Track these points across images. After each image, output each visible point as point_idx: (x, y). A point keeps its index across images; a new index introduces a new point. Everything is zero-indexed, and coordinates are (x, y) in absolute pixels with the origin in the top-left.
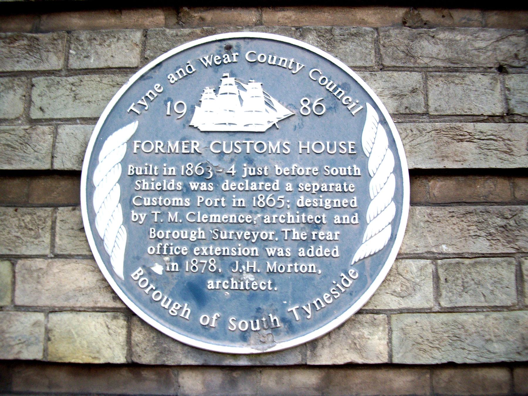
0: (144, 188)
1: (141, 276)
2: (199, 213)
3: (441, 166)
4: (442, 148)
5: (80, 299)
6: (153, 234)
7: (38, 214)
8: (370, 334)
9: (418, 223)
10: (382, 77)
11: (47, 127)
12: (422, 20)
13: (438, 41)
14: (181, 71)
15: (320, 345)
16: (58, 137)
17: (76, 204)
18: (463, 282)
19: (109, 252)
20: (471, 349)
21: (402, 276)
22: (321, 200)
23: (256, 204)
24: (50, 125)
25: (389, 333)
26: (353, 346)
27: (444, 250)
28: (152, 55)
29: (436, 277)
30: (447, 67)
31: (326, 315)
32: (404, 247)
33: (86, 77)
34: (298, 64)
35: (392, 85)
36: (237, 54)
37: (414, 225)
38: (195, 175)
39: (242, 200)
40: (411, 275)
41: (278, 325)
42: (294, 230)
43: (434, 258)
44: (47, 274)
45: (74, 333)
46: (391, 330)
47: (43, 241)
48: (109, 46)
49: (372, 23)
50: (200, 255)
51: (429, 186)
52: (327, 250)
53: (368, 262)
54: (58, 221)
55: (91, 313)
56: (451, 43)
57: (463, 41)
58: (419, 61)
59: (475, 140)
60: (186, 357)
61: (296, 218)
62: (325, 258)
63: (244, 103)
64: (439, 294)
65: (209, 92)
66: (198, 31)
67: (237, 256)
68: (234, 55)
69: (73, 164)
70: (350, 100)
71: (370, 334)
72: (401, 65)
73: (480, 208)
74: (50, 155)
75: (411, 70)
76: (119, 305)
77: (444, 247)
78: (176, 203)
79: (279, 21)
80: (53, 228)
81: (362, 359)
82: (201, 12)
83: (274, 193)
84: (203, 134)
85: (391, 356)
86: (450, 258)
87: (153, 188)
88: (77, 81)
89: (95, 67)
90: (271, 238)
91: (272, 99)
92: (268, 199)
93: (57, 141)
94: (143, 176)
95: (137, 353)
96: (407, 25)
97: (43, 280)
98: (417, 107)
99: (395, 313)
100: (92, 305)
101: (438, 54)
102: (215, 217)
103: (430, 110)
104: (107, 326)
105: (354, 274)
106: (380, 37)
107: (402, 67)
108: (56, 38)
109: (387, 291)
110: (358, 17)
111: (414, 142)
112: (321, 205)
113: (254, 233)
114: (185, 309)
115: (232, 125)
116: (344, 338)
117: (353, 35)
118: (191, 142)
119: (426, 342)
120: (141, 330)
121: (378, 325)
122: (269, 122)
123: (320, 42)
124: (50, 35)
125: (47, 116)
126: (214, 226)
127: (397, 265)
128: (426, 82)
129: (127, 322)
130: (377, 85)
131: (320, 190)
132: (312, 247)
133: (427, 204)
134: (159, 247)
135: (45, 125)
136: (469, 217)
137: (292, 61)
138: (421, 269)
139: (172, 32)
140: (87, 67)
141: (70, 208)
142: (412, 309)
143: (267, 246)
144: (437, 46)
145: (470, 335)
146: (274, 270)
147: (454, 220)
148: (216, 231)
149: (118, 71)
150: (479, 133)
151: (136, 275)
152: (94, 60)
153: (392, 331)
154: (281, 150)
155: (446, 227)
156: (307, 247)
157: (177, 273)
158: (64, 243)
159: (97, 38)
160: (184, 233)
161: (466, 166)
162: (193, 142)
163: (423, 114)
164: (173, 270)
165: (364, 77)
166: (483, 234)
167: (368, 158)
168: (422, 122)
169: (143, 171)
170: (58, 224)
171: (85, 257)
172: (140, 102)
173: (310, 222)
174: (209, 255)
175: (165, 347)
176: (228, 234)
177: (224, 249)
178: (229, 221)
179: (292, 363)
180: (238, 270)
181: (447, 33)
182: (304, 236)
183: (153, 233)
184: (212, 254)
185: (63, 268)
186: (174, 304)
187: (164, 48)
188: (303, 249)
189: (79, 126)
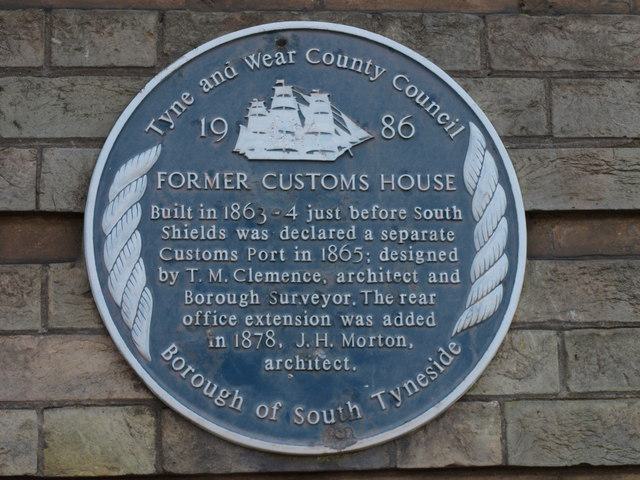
0: (174, 237)
3: (568, 207)
4: (571, 182)
6: (189, 299)
7: (21, 273)
8: (478, 427)
13: (568, 34)
15: (413, 443)
17: (76, 256)
18: (598, 360)
20: (610, 446)
22: (411, 252)
28: (173, 49)
29: (563, 354)
31: (422, 401)
32: (521, 313)
33: (80, 79)
39: (307, 255)
43: (560, 328)
46: (504, 423)
47: (30, 311)
48: (111, 34)
49: (476, 6)
53: (473, 333)
54: (50, 283)
56: (584, 38)
57: (601, 34)
58: (540, 63)
59: (615, 172)
61: (378, 276)
63: (306, 122)
65: (257, 106)
66: (237, 16)
68: (290, 53)
70: (448, 118)
71: (478, 427)
73: (622, 262)
76: (142, 395)
77: (573, 313)
80: (44, 292)
84: (251, 164)
85: (505, 456)
87: (186, 237)
90: (346, 303)
91: (343, 116)
92: (341, 251)
96: (525, 8)
100: (105, 396)
101: (567, 53)
102: (272, 275)
104: (128, 425)
105: (456, 348)
107: (517, 71)
108: (29, 19)
112: (411, 259)
117: (451, 26)
122: (340, 148)
124: (19, 13)
126: (271, 287)
131: (409, 238)
132: (401, 314)
134: (198, 316)
135: (23, 147)
136: (606, 275)
137: (369, 63)
140: (80, 65)
141: (68, 264)
143: (341, 313)
144: (565, 41)
145: (609, 428)
146: (351, 343)
147: (586, 278)
150: (621, 163)
156: (394, 314)
158: (63, 312)
160: (232, 296)
161: (601, 206)
162: (238, 174)
164: (218, 345)
166: (626, 297)
167: (472, 197)
169: (172, 213)
170: (51, 286)
171: (92, 332)
172: (162, 118)
174: (266, 325)
176: (290, 298)
177: (285, 317)
179: (377, 466)
180: (305, 345)
181: (579, 23)
182: (390, 300)
185: (62, 347)
186: (222, 391)
189: (74, 149)
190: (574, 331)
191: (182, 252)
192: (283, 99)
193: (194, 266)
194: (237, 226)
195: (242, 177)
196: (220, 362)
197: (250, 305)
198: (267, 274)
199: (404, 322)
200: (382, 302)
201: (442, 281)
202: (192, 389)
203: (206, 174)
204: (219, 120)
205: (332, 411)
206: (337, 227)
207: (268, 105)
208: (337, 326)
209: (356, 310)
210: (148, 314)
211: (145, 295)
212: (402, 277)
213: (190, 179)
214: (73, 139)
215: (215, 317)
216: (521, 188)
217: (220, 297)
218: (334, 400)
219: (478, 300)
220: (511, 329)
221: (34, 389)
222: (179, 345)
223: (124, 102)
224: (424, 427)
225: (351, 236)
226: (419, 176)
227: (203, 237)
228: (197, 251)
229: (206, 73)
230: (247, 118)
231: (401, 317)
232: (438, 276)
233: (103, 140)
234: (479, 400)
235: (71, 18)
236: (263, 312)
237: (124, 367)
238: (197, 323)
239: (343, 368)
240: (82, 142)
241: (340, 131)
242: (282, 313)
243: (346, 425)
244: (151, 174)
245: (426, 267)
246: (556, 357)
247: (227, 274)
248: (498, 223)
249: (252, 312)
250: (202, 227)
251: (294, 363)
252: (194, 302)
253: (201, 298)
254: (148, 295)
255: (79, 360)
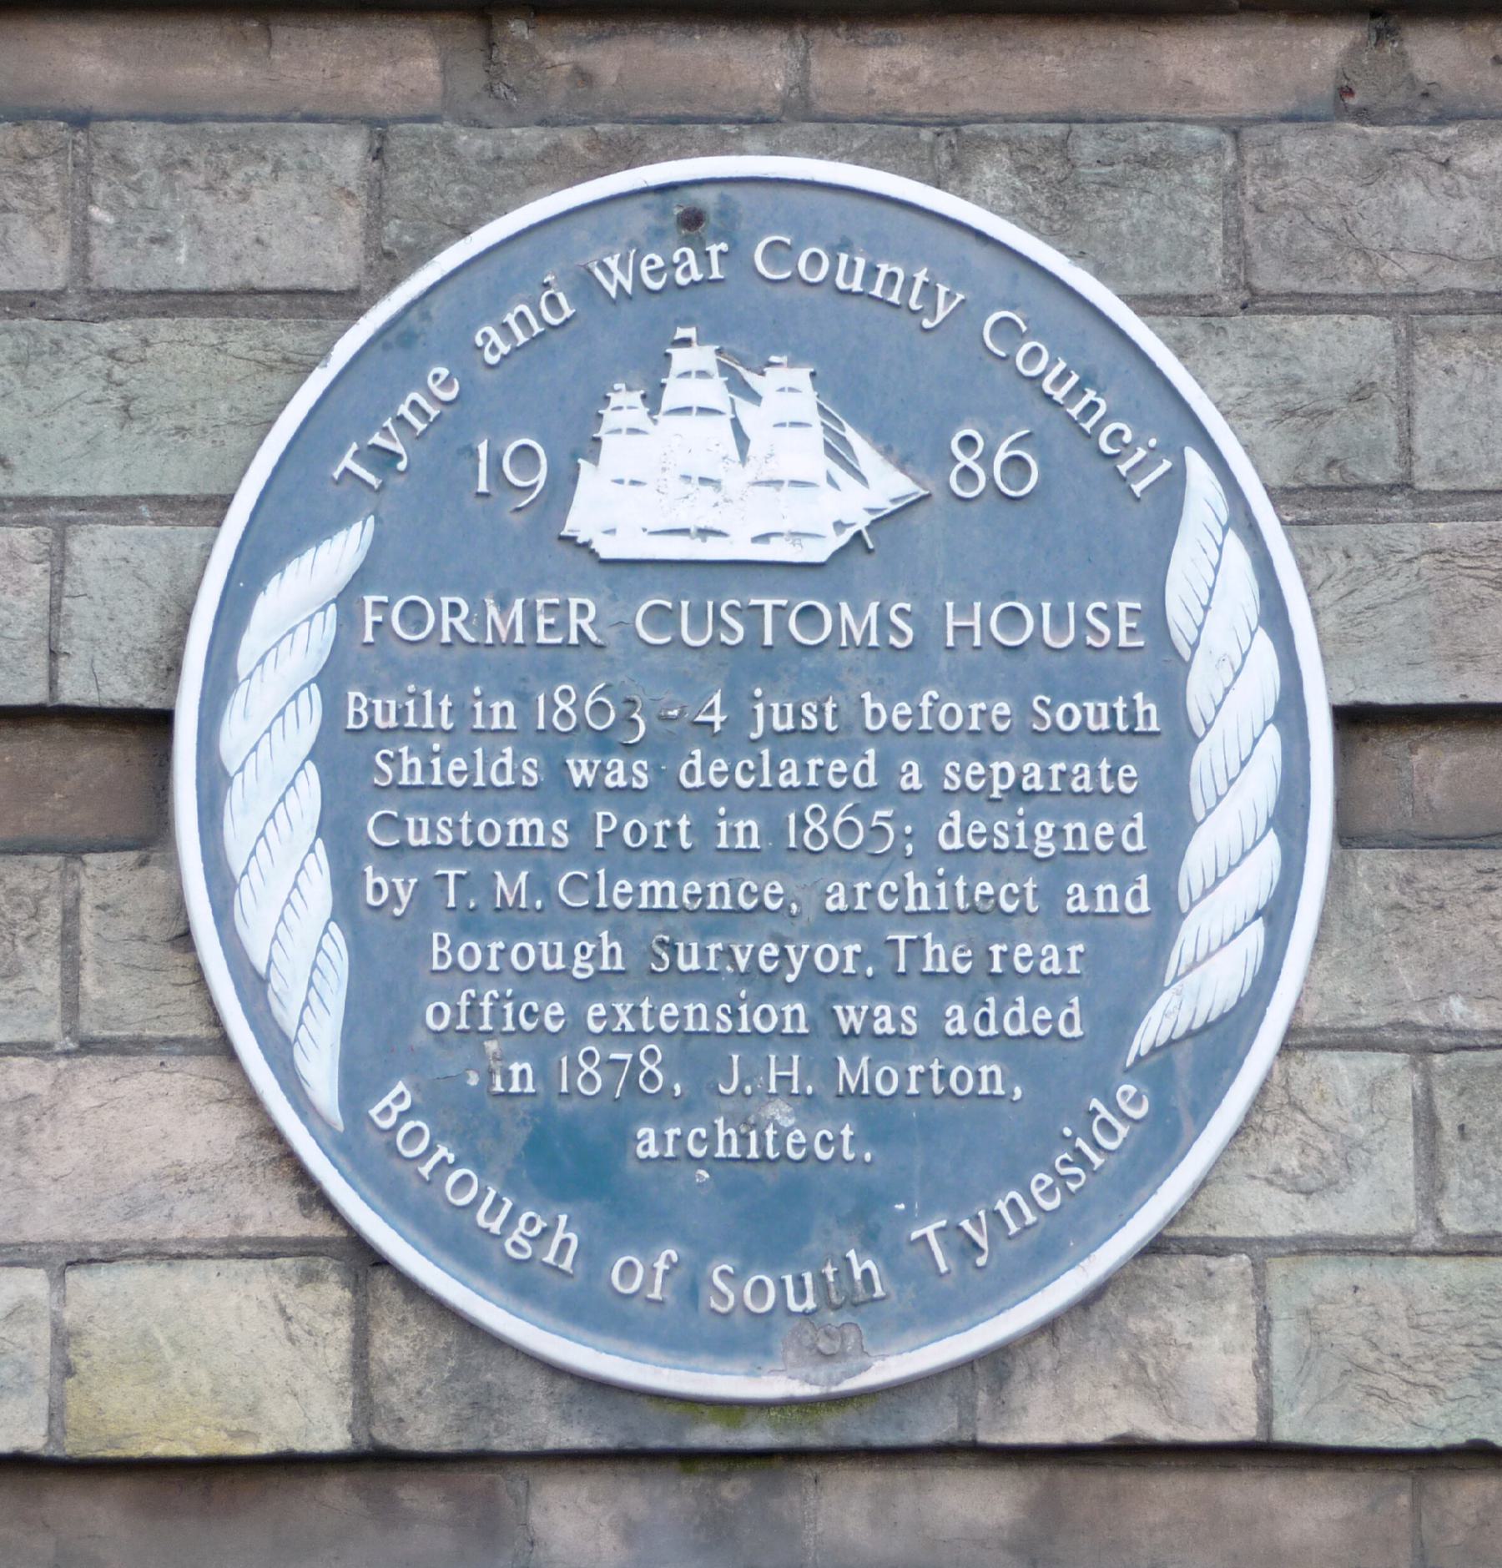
0: (405, 781)
1: (404, 1116)
2: (601, 872)
3: (1449, 694)
4: (1459, 621)
5: (181, 1209)
9: (1364, 910)
10: (1245, 339)
11: (26, 532)
12: (1412, 80)
13: (1463, 180)
14: (521, 315)
15: (1021, 1372)
16: (68, 572)
17: (151, 834)
19: (289, 1024)
21: (1303, 1112)
22: (1021, 825)
23: (799, 838)
24: (36, 522)
25: (1259, 1326)
26: (1132, 1374)
27: (1457, 1018)
29: (1426, 1120)
30: (1489, 294)
31: (1045, 1252)
33: (164, 328)
34: (943, 290)
35: (1282, 370)
36: (724, 246)
37: (1349, 918)
38: (583, 728)
39: (747, 831)
40: (1336, 1108)
41: (879, 1292)
42: (928, 937)
44: (54, 1115)
45: (162, 1341)
46: (1265, 1318)
47: (33, 989)
48: (244, 195)
49: (1223, 99)
50: (607, 1030)
51: (1411, 770)
52: (1043, 1012)
53: (1183, 1058)
54: (86, 908)
55: (222, 1263)
60: (566, 1418)
61: (934, 893)
62: (1033, 1042)
64: (1438, 1184)
65: (624, 406)
66: (575, 139)
67: (734, 1033)
68: (714, 249)
69: (135, 684)
70: (1127, 438)
71: (1197, 1329)
72: (1319, 289)
74: (45, 643)
75: (1355, 305)
76: (320, 1228)
77: (1457, 1005)
78: (519, 837)
79: (871, 92)
80: (69, 936)
81: (1167, 1423)
82: (579, 43)
83: (859, 800)
85: (1266, 1415)
86: (1477, 1048)
87: (437, 781)
88: (132, 341)
89: (194, 284)
90: (849, 968)
91: (850, 434)
92: (839, 820)
93: (67, 588)
94: (401, 734)
95: (391, 1411)
96: (1353, 102)
97: (39, 1140)
98: (1370, 461)
99: (1281, 1251)
100: (223, 1231)
102: (659, 890)
103: (1418, 471)
104: (282, 1310)
105: (1136, 1101)
106: (1247, 171)
108: (32, 151)
109: (1253, 1171)
110: (1170, 71)
111: (1359, 601)
112: (1021, 845)
113: (790, 949)
114: (559, 1236)
115: (711, 539)
116: (1105, 1342)
117: (1144, 162)
118: (568, 603)
119: (1389, 1365)
120: (404, 1321)
121: (1222, 1296)
122: (839, 526)
123: (1024, 194)
125: (22, 488)
127: (1287, 1072)
128: (1409, 355)
129: (354, 1293)
130: (1226, 372)
132: (991, 1000)
133: (1401, 842)
134: (464, 1003)
137: (921, 276)
138: (1373, 1088)
139: (479, 142)
140: (164, 286)
141: (132, 857)
142: (1342, 1239)
143: (836, 998)
144: (1456, 204)
146: (860, 1085)
148: (662, 943)
149: (283, 302)
151: (387, 1110)
152: (191, 256)
153: (1270, 1319)
154: (882, 636)
155: (1465, 931)
156: (973, 1003)
157: (529, 1099)
158: (117, 995)
159: (195, 159)
160: (552, 948)
162: (574, 602)
163: (1392, 486)
165: (1180, 340)
168: (1388, 520)
169: (401, 713)
171: (192, 1047)
172: (377, 439)
173: (981, 906)
174: (639, 1032)
175: (488, 1384)
176: (703, 953)
177: (690, 1008)
178: (705, 903)
179: (925, 1435)
180: (740, 1088)
182: (963, 960)
183: (445, 949)
184: (647, 1028)
187: (451, 210)
188: (960, 1009)
189: (148, 529)
190: (1457, 1056)
191: (425, 821)
192: (693, 383)
193: (457, 863)
194: (568, 748)
195: (583, 609)
196: (521, 1135)
197: (599, 972)
198: (645, 886)
199: (999, 1023)
200: (943, 968)
201: (1101, 908)
202: (445, 1210)
203: (489, 602)
204: (525, 447)
205: (808, 1277)
206: (829, 754)
207: (652, 401)
208: (824, 1040)
209: (875, 988)
210: (336, 999)
211: (328, 945)
212: (996, 896)
213: (447, 618)
214: (145, 498)
215: (509, 1006)
216: (1322, 642)
217: (523, 952)
218: (815, 1246)
219: (1195, 964)
220: (1286, 1048)
221: (42, 1210)
222: (416, 1088)
223: (278, 395)
224: (1049, 1327)
225: (865, 778)
226: (1046, 606)
227: (480, 782)
228: (465, 820)
229: (493, 312)
230: (598, 440)
231: (991, 1011)
232: (1091, 894)
233: (224, 502)
234: (1200, 1252)
235: (141, 147)
236: (634, 993)
237: (274, 1150)
238: (463, 1025)
239: (838, 1154)
240: (171, 507)
241: (840, 474)
242: (681, 996)
243: (847, 1317)
244: (347, 599)
245: (1060, 867)
246: (1409, 1130)
247: (541, 885)
248: (1256, 741)
249: (606, 994)
250: (479, 752)
251: (711, 1139)
252: (455, 965)
253: (472, 954)
254: (337, 946)
255: (159, 1124)
